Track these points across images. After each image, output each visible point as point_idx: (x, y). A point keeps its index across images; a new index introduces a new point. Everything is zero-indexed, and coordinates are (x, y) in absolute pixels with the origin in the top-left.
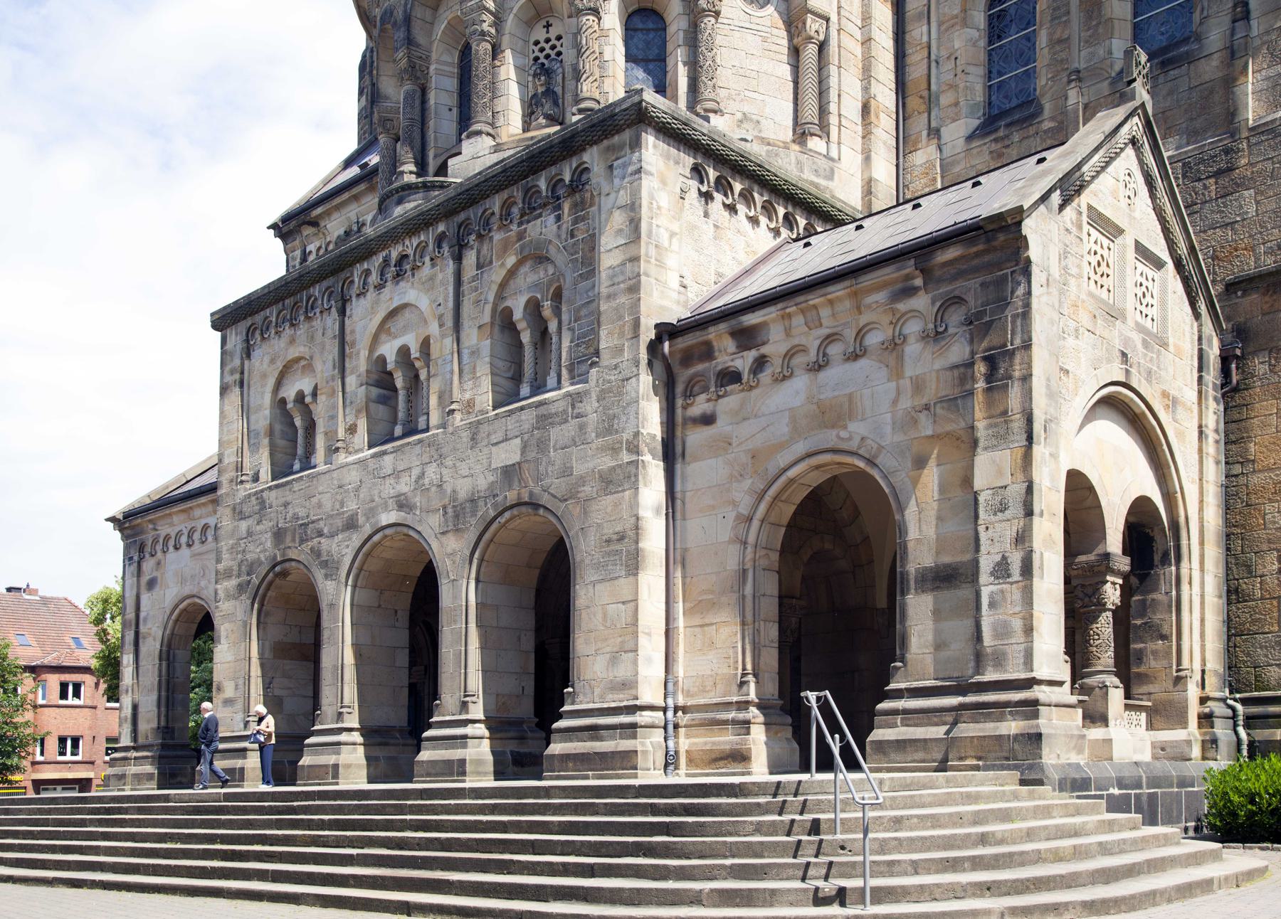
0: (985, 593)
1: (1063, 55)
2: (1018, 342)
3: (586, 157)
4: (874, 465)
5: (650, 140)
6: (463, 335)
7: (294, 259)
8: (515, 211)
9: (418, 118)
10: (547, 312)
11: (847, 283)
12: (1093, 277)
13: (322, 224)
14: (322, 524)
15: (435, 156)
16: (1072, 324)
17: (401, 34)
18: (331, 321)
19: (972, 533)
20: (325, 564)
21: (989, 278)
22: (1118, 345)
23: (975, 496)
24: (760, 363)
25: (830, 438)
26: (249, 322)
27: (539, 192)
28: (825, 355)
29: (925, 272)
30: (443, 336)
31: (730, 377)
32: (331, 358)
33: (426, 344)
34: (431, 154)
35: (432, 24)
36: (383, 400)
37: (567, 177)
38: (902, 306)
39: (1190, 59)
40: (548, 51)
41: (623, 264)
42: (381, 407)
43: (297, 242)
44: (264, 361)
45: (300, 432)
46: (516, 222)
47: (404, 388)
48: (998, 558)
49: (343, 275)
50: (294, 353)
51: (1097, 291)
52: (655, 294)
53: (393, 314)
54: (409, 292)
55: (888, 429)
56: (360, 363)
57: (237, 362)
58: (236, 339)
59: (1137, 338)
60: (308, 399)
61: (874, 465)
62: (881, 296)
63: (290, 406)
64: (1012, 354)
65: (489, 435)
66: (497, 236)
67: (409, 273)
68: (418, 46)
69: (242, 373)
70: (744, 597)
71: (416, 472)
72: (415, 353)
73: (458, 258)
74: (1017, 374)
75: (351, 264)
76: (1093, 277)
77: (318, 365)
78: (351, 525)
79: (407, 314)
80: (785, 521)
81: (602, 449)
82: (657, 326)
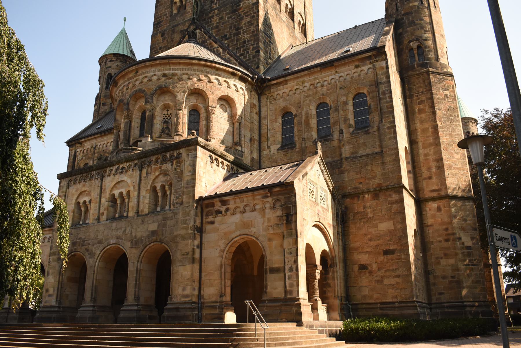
0: (287, 275)
1: (301, 134)
2: (293, 212)
3: (181, 151)
4: (258, 239)
5: (199, 148)
6: (141, 192)
7: (72, 153)
8: (159, 160)
9: (128, 129)
10: (167, 188)
11: (251, 193)
12: (310, 195)
13: (83, 144)
14: (90, 241)
15: (133, 139)
16: (306, 208)
17: (126, 107)
18: (98, 182)
19: (283, 259)
20: (90, 254)
21: (286, 196)
22: (317, 212)
23: (284, 249)
24: (227, 210)
25: (246, 231)
26: (70, 178)
27: (167, 157)
28: (245, 209)
29: (271, 193)
30: (134, 191)
31: (219, 212)
32: (97, 192)
33: (129, 192)
34: (131, 139)
35: (135, 105)
36: (112, 206)
37: (175, 155)
38: (265, 200)
39: (331, 140)
40: (167, 117)
41: (191, 180)
42: (112, 208)
43: (74, 148)
44: (74, 190)
45: (83, 213)
46: (159, 163)
47: (120, 204)
48: (290, 266)
49: (103, 170)
50: (84, 189)
51: (311, 199)
52: (199, 188)
53: (118, 183)
54: (125, 177)
55: (262, 230)
56: (107, 195)
57: (64, 189)
58: (65, 183)
59: (321, 210)
60: (87, 203)
61: (258, 239)
62: (259, 197)
63: (81, 204)
64: (292, 215)
65: (148, 221)
66: (153, 167)
67: (125, 172)
68: (130, 110)
69: (66, 193)
70: (222, 272)
71: (123, 229)
72: (125, 194)
73: (141, 171)
74: (293, 220)
75: (107, 167)
76: (310, 195)
77: (92, 194)
78: (100, 242)
79: (123, 183)
80: (233, 252)
81: (183, 228)
82: (199, 197)
